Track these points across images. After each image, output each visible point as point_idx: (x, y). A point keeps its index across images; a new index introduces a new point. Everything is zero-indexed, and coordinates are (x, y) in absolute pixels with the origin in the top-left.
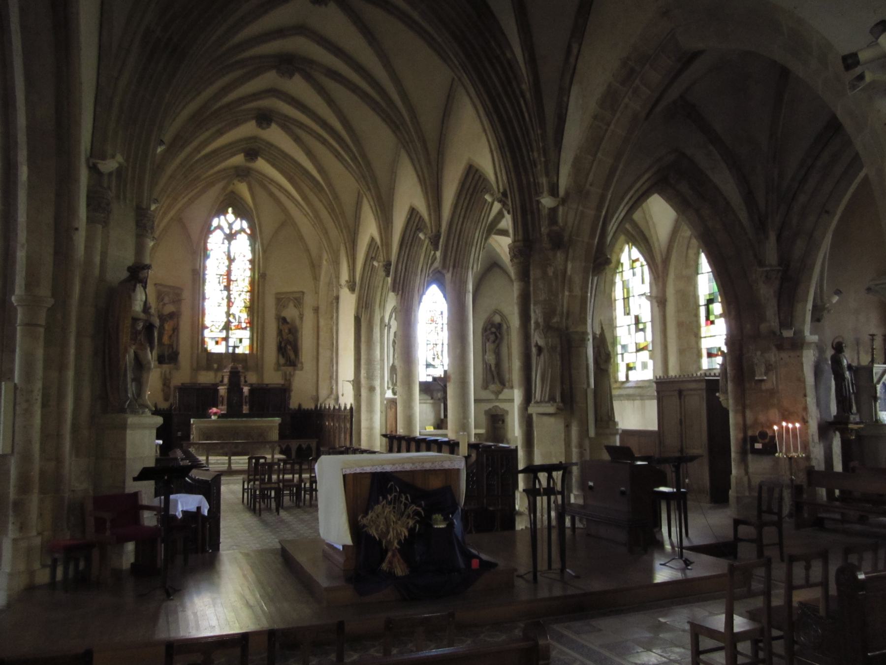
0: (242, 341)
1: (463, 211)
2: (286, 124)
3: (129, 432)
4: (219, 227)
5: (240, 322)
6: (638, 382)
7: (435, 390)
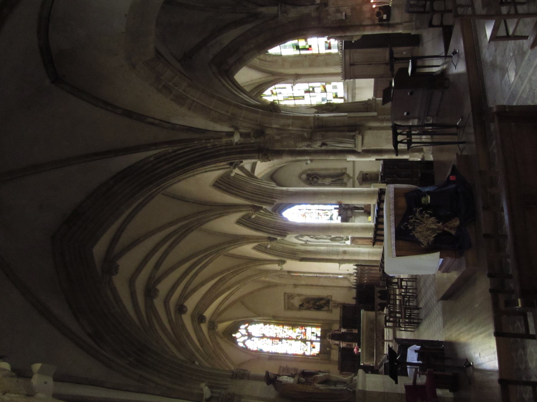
0: (313, 332)
1: (239, 191)
2: (184, 297)
3: (367, 389)
4: (244, 342)
5: (302, 333)
6: (344, 92)
7: (346, 212)
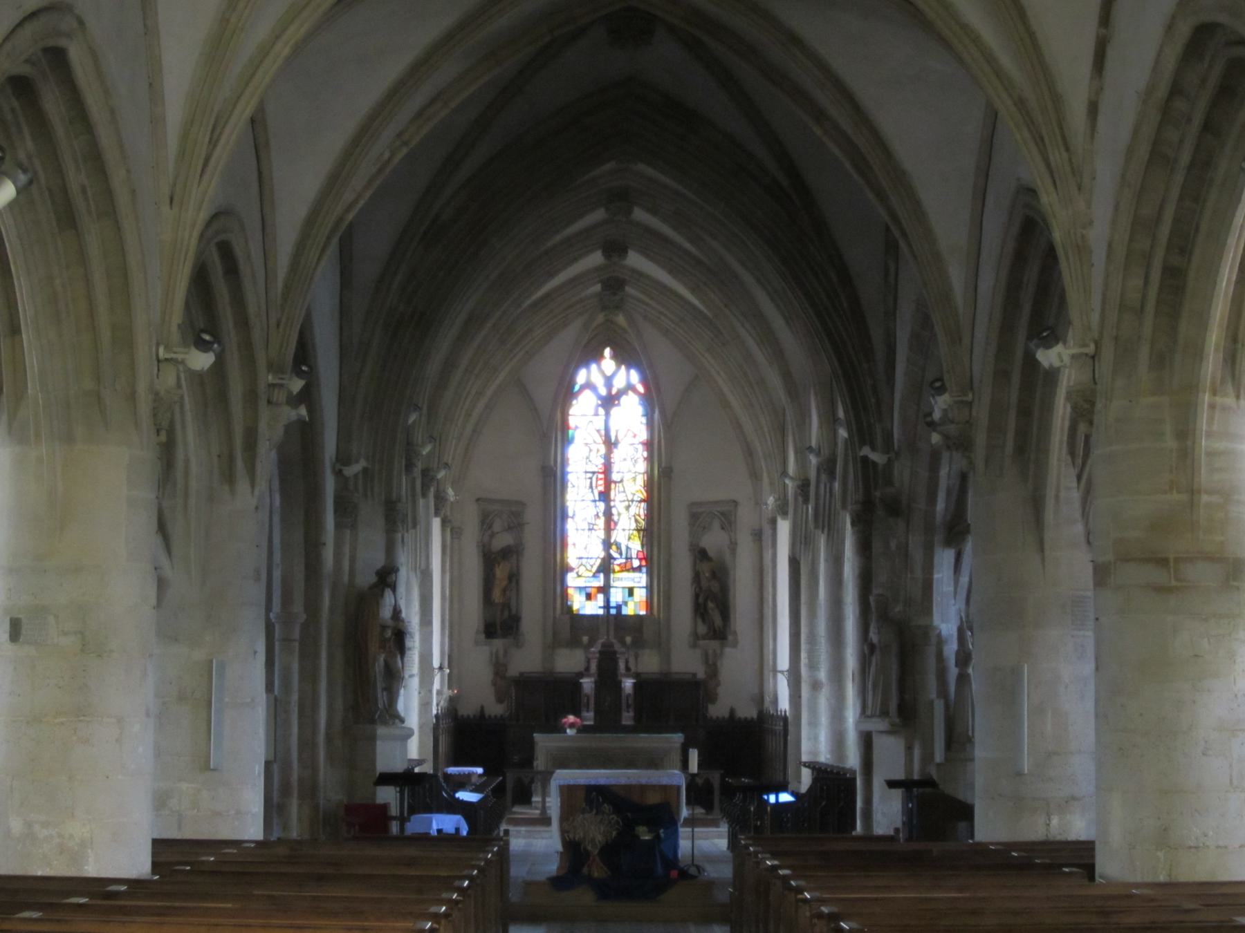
0: (631, 593)
3: (379, 743)
5: (629, 558)
